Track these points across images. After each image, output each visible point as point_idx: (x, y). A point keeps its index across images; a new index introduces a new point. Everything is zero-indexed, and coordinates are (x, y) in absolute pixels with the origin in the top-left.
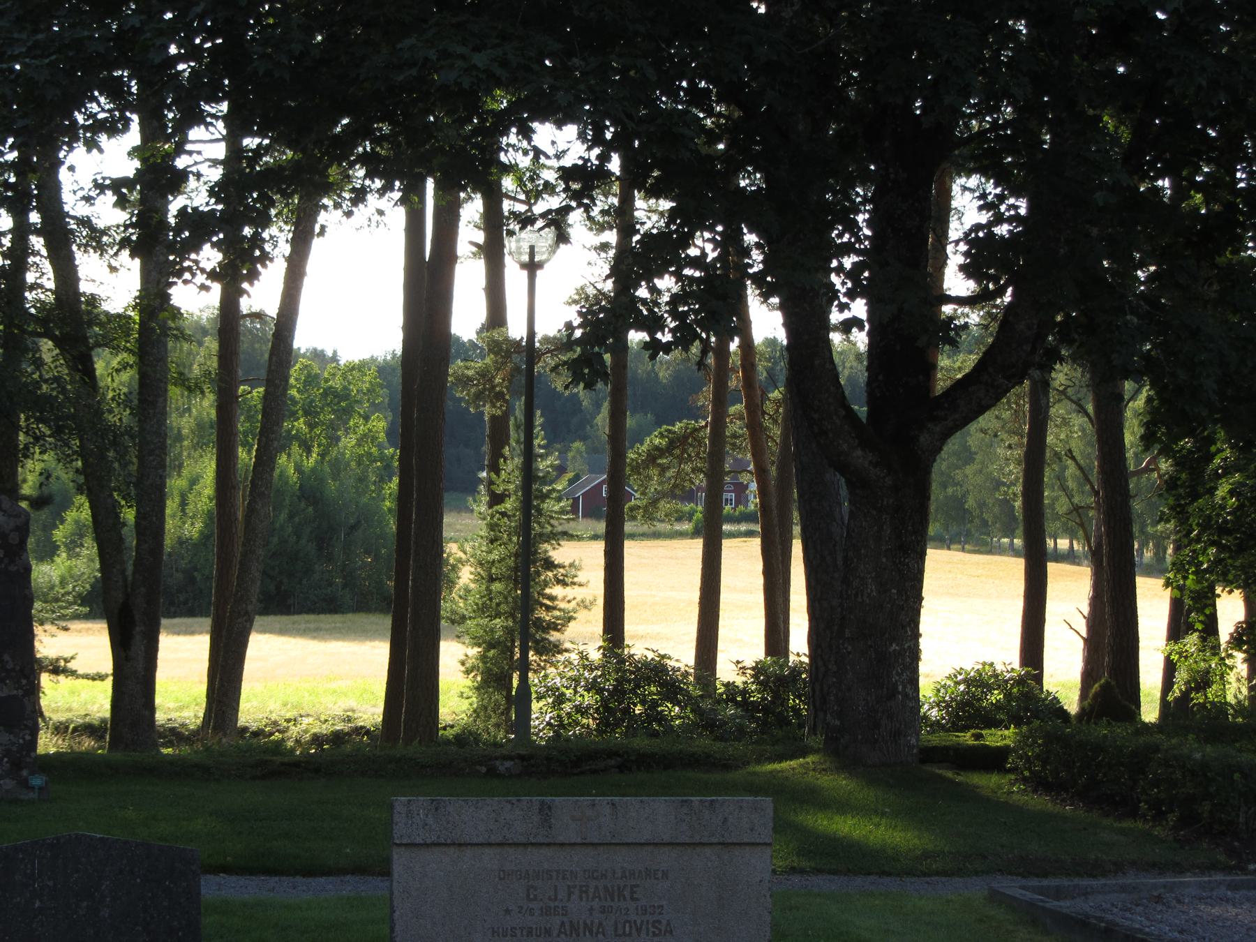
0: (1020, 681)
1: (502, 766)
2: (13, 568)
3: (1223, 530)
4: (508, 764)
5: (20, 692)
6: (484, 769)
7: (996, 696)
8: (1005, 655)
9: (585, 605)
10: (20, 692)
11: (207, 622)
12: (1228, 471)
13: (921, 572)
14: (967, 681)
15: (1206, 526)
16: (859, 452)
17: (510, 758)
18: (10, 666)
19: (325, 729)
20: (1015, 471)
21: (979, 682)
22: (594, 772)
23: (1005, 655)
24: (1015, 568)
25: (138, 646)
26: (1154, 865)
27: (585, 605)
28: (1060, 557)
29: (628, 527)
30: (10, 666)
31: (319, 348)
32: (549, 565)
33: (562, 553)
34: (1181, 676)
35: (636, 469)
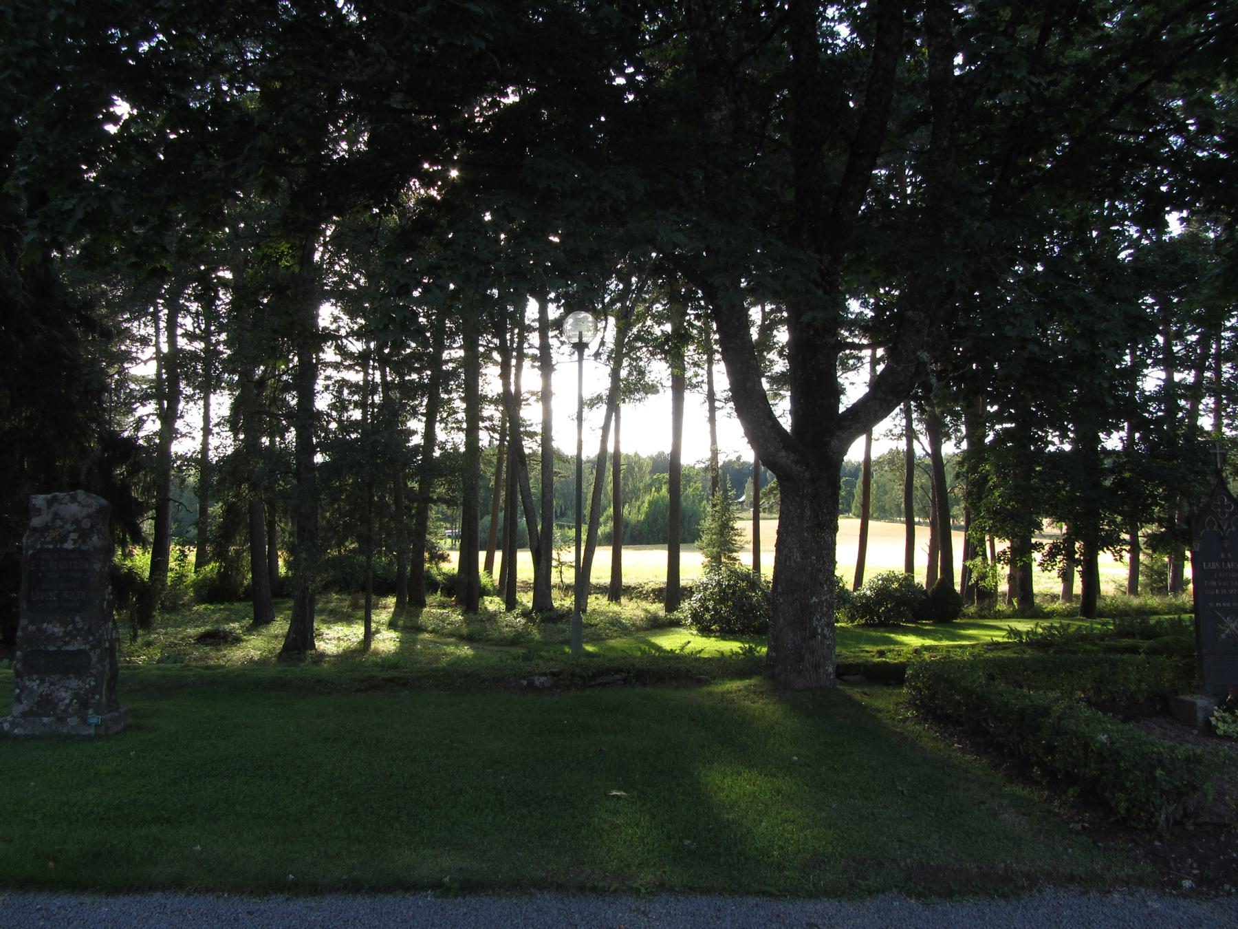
0: (906, 579)
1: (538, 681)
2: (84, 548)
3: (996, 513)
4: (542, 679)
5: (88, 647)
6: (525, 683)
7: (895, 585)
8: (899, 568)
9: (747, 542)
10: (88, 647)
11: (666, 546)
12: (995, 487)
13: (834, 543)
14: (883, 579)
15: (988, 510)
16: (783, 453)
17: (545, 674)
18: (80, 625)
19: (657, 587)
20: (901, 494)
21: (888, 580)
22: (604, 685)
23: (899, 568)
24: (902, 528)
25: (543, 565)
26: (1072, 878)
27: (747, 542)
28: (919, 523)
29: (762, 515)
30: (80, 625)
31: (655, 454)
32: (733, 529)
33: (738, 525)
34: (974, 575)
35: (765, 495)
